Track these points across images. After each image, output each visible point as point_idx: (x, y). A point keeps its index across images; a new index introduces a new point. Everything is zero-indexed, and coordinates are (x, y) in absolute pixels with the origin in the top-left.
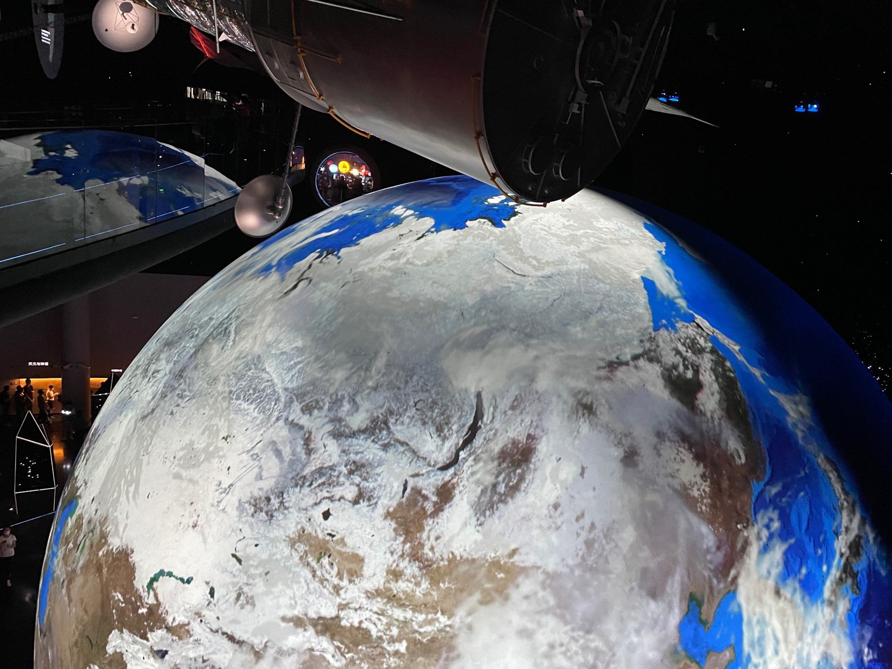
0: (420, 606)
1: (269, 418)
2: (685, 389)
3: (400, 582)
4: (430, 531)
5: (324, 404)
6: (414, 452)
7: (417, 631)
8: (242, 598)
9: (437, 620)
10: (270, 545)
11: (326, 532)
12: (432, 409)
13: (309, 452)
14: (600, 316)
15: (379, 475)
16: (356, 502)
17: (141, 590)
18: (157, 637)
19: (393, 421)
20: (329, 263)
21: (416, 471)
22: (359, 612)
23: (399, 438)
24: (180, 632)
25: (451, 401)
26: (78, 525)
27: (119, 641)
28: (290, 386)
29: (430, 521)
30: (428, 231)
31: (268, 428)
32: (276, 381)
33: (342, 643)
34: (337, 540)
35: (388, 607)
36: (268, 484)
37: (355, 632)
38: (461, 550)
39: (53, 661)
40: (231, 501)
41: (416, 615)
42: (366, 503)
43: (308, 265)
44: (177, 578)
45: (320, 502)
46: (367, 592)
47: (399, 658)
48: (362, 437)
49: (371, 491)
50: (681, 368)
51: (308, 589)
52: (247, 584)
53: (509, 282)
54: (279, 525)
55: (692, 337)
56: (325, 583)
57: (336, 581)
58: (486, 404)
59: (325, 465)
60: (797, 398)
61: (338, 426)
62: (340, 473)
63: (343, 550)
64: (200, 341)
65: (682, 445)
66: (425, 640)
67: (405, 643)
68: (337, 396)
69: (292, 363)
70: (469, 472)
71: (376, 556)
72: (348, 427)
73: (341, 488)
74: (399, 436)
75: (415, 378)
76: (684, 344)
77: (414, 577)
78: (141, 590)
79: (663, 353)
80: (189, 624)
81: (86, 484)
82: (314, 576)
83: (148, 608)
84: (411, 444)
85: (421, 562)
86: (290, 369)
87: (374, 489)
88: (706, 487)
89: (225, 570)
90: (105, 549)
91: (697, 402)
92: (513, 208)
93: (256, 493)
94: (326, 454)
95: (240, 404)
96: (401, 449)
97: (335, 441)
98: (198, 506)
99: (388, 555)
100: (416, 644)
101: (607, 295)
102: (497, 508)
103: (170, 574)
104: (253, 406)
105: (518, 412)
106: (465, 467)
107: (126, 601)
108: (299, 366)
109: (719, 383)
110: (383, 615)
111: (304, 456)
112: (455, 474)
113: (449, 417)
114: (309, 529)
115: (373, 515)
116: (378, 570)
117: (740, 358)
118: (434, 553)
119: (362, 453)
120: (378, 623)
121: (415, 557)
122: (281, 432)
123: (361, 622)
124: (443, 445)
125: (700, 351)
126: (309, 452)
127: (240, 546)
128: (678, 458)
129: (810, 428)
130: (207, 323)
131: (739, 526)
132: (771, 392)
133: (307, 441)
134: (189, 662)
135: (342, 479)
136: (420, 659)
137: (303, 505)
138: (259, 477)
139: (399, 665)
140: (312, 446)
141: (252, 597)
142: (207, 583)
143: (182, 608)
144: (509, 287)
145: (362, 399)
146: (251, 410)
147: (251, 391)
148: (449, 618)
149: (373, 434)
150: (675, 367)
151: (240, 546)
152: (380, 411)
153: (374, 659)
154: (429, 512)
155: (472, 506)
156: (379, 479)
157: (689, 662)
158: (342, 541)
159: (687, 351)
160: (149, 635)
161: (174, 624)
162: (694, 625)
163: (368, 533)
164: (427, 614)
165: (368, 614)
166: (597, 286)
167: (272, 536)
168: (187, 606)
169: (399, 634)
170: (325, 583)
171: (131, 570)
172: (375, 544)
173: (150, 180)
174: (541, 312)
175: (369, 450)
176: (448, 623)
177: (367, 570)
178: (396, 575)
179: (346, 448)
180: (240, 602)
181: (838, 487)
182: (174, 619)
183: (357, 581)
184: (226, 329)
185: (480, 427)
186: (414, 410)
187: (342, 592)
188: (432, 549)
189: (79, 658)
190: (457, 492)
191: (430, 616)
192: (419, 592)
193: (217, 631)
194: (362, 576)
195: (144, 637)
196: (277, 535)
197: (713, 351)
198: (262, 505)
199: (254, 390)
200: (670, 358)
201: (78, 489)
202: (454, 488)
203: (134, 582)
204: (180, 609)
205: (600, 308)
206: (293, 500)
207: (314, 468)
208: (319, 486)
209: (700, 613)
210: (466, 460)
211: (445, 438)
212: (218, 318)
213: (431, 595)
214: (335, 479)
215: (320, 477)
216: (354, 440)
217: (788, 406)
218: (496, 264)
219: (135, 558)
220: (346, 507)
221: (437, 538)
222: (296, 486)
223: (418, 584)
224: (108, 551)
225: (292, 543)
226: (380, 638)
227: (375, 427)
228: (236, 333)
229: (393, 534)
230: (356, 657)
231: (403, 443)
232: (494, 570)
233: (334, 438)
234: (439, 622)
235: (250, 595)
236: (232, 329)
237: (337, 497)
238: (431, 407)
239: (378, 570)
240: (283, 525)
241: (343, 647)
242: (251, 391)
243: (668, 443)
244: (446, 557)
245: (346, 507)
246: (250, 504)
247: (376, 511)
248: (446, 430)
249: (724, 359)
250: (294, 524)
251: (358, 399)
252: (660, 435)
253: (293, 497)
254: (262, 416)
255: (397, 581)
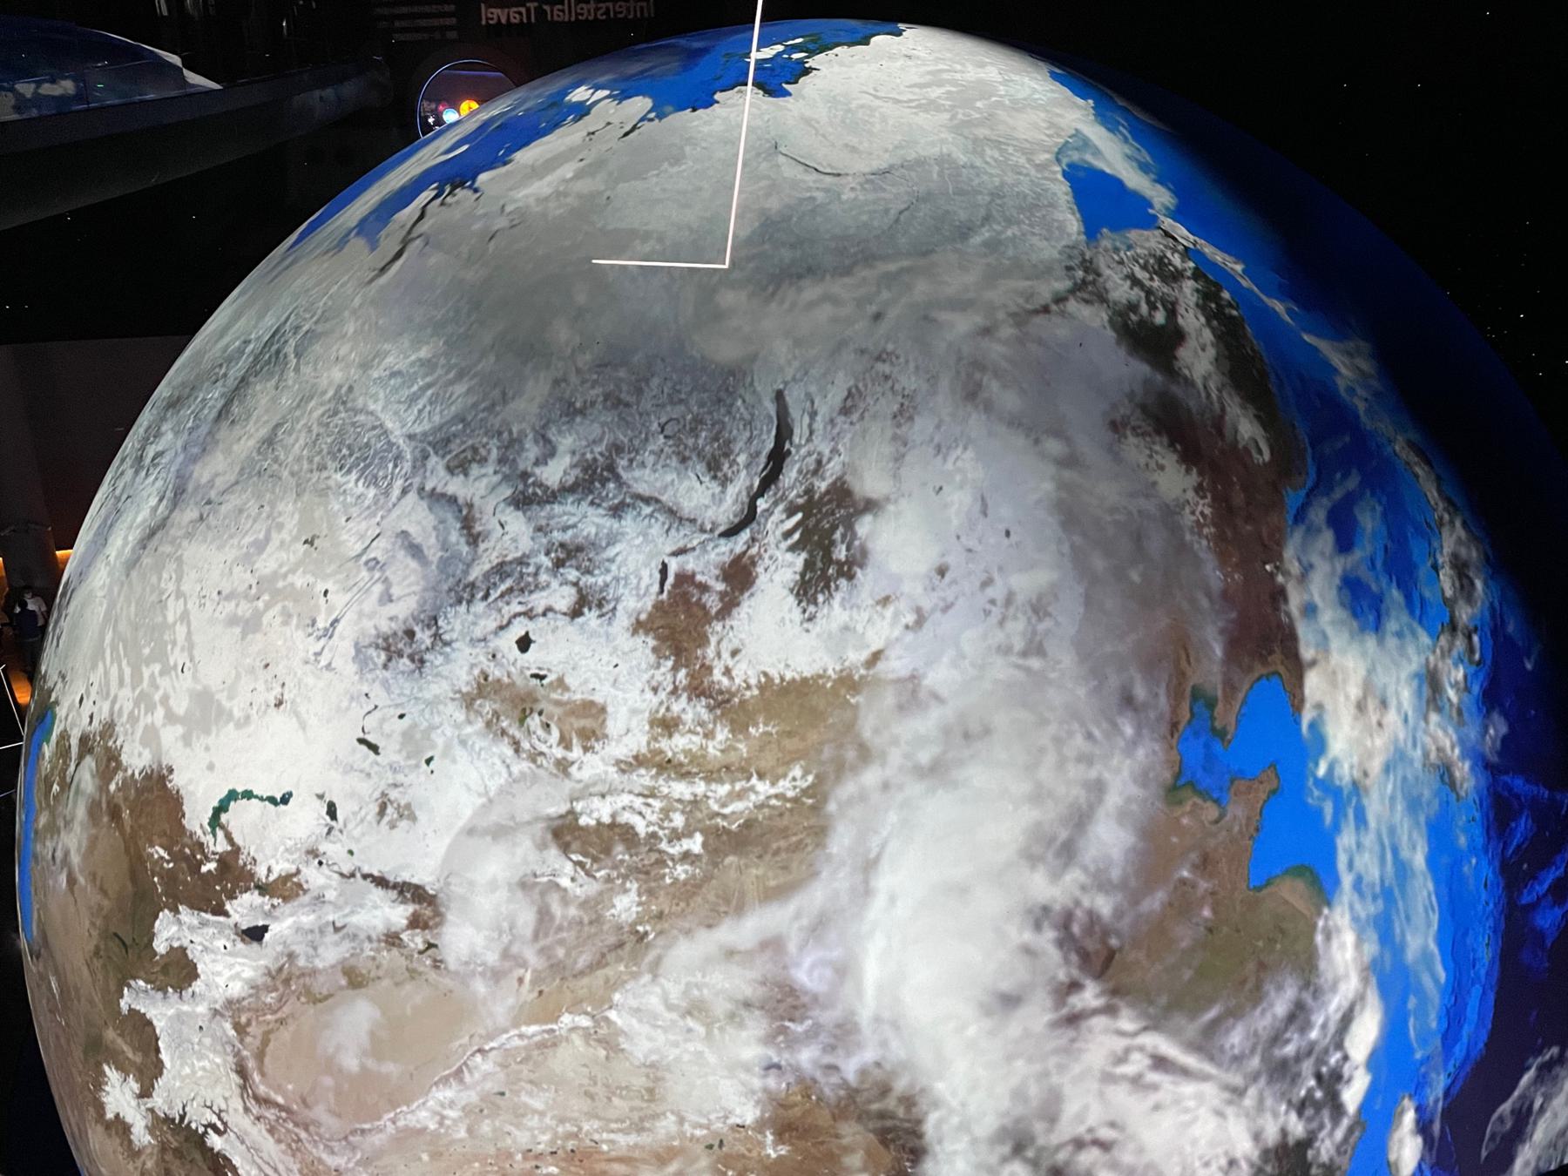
0: (719, 771)
1: (387, 494)
2: (1153, 341)
3: (676, 737)
4: (719, 643)
5: (489, 451)
6: (671, 512)
7: (718, 814)
8: (390, 810)
9: (752, 789)
10: (427, 711)
11: (528, 673)
12: (694, 432)
13: (474, 539)
14: (986, 233)
15: (611, 560)
16: (575, 613)
17: (199, 832)
18: (245, 908)
19: (624, 463)
20: (457, 202)
21: (681, 544)
22: (609, 798)
23: (640, 491)
24: (285, 889)
25: (729, 413)
26: (63, 751)
27: (175, 928)
28: (418, 429)
29: (718, 626)
30: (642, 120)
31: (390, 511)
32: (389, 425)
33: (585, 855)
34: (551, 683)
35: (661, 782)
36: (405, 608)
37: (606, 834)
38: (782, 666)
39: (61, 992)
40: (342, 646)
41: (713, 786)
42: (595, 612)
43: (417, 214)
44: (261, 799)
45: (509, 623)
46: (618, 762)
47: (692, 863)
48: (570, 499)
49: (601, 591)
50: (1144, 308)
51: (510, 774)
52: (396, 786)
53: (809, 189)
54: (438, 675)
55: (1159, 253)
56: (540, 760)
57: (559, 752)
58: (795, 413)
59: (509, 558)
60: (1351, 345)
61: (521, 487)
62: (538, 568)
63: (566, 697)
64: (231, 382)
65: (1157, 439)
66: (734, 827)
67: (699, 838)
68: (510, 433)
69: (415, 388)
70: (779, 533)
71: (626, 700)
72: (541, 485)
73: (544, 594)
74: (642, 488)
75: (655, 382)
76: (1144, 267)
77: (702, 724)
78: (199, 832)
79: (1109, 285)
80: (298, 872)
81: (63, 677)
82: (517, 751)
83: (218, 861)
84: (664, 498)
85: (711, 697)
86: (413, 399)
87: (607, 585)
88: (1204, 507)
89: (349, 769)
90: (119, 776)
91: (1177, 365)
92: (801, 62)
93: (386, 627)
94: (506, 538)
95: (328, 478)
96: (647, 510)
97: (520, 514)
98: (279, 669)
99: (649, 695)
100: (719, 836)
101: (996, 194)
102: (837, 588)
103: (248, 795)
104: (354, 476)
105: (855, 417)
106: (769, 526)
107: (174, 857)
108: (429, 392)
109: (1213, 330)
110: (653, 796)
111: (465, 549)
112: (753, 540)
113: (728, 442)
114: (496, 673)
115: (610, 630)
116: (634, 723)
117: (1246, 283)
118: (732, 678)
119: (574, 526)
120: (647, 811)
121: (698, 689)
122: (416, 518)
123: (613, 816)
124: (723, 492)
125: (1175, 277)
126: (474, 539)
127: (371, 722)
128: (1153, 465)
129: (1377, 394)
130: (241, 351)
131: (1268, 567)
132: (1306, 337)
133: (467, 523)
134: (310, 937)
135: (543, 577)
136: (730, 859)
137: (478, 632)
138: (387, 598)
139: (694, 876)
140: (478, 528)
141: (408, 806)
142: (320, 797)
143: (282, 848)
144: (813, 199)
145: (560, 432)
146: (351, 484)
147: (345, 451)
148: (773, 784)
149: (591, 492)
150: (1133, 307)
151: (371, 722)
152: (598, 449)
153: (647, 873)
154: (714, 611)
155: (792, 590)
156: (614, 567)
157: (1199, 801)
158: (561, 683)
159: (1152, 279)
160: (228, 907)
161: (271, 878)
162: (1203, 739)
163: (608, 665)
164: (733, 782)
165: (626, 799)
166: (976, 182)
167: (427, 695)
168: (290, 843)
169: (687, 824)
170: (540, 760)
171: (174, 803)
172: (622, 679)
173: (77, 87)
174: (877, 237)
175: (587, 520)
176: (773, 791)
177: (614, 726)
178: (667, 725)
179: (543, 522)
180: (386, 819)
181: (1433, 494)
182: (269, 870)
183: (598, 747)
184: (278, 352)
185: (789, 452)
186: (661, 439)
187: (573, 770)
188: (727, 672)
189: (106, 978)
190: (760, 569)
191: (738, 786)
192: (713, 749)
193: (353, 875)
194: (606, 736)
195: (220, 911)
196: (438, 691)
197: (1197, 275)
198: (401, 646)
199: (349, 447)
200: (1121, 292)
201: (50, 691)
202: (754, 564)
203: (184, 822)
204: (276, 849)
205: (987, 219)
206: (458, 627)
207: (487, 567)
208: (502, 596)
209: (1212, 718)
210: (769, 512)
211: (725, 482)
212: (258, 338)
213: (736, 749)
214: (530, 579)
215: (502, 580)
216: (556, 506)
217: (1337, 359)
218: (781, 159)
219: (177, 781)
220: (559, 623)
221: (734, 653)
222: (460, 602)
223: (709, 735)
224: (124, 780)
225: (468, 701)
226: (654, 835)
227: (593, 479)
228: (298, 355)
229: (652, 658)
230: (615, 874)
231: (647, 500)
232: (843, 691)
233: (517, 508)
234: (757, 793)
235: (403, 803)
236: (289, 349)
237: (540, 610)
238: (692, 430)
239: (634, 723)
240: (445, 673)
241: (588, 861)
242: (345, 451)
243: (1132, 440)
244: (753, 681)
245: (559, 623)
246: (377, 647)
247: (616, 623)
248: (726, 466)
249: (1219, 288)
250: (466, 668)
251: (552, 433)
252: (1116, 426)
253: (455, 622)
254: (372, 492)
255: (670, 736)
